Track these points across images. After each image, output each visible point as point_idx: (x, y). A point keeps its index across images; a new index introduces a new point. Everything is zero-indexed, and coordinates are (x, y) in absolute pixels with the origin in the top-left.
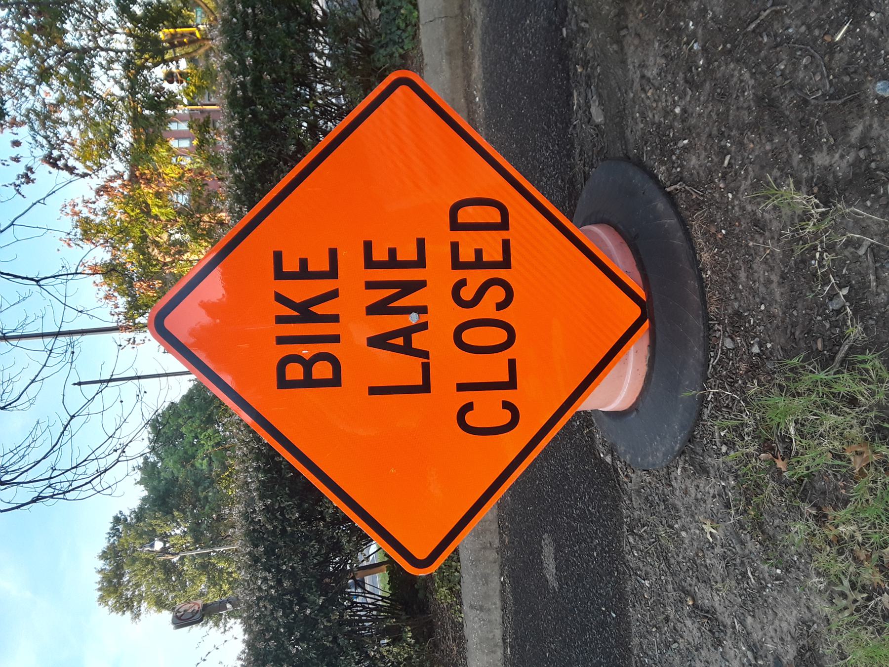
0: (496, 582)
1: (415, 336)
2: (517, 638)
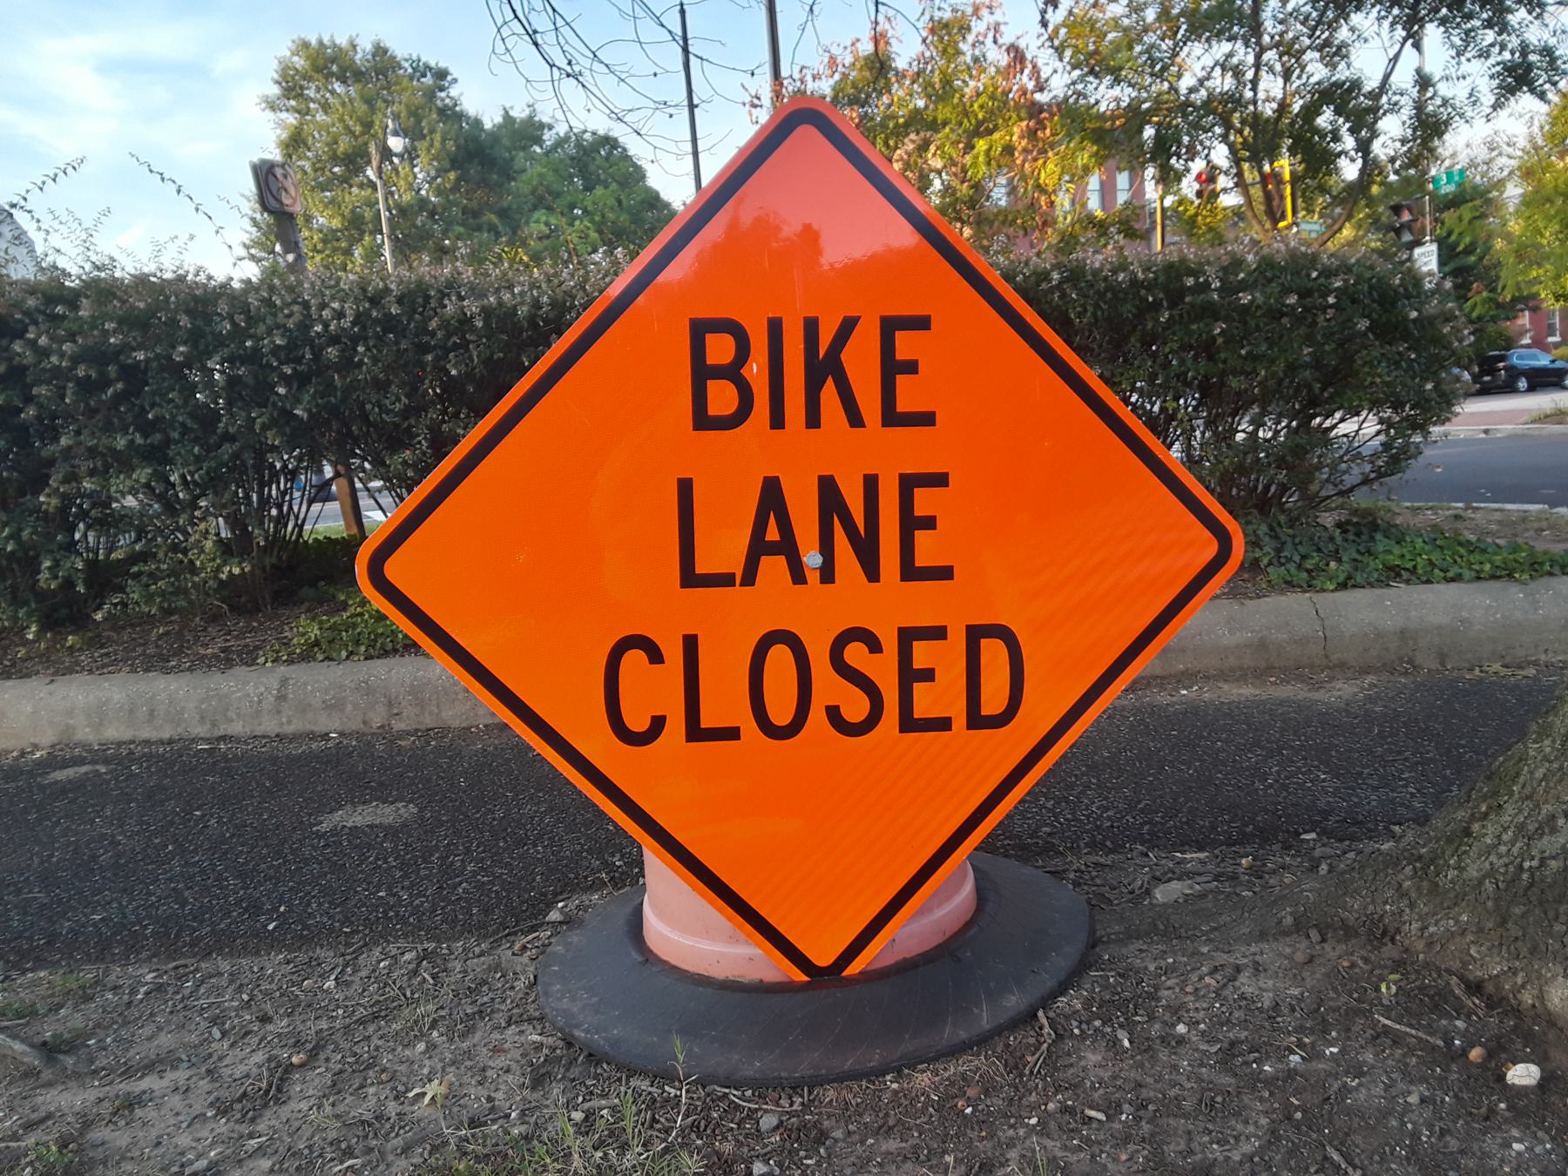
0: (331, 724)
1: (781, 562)
2: (227, 760)
